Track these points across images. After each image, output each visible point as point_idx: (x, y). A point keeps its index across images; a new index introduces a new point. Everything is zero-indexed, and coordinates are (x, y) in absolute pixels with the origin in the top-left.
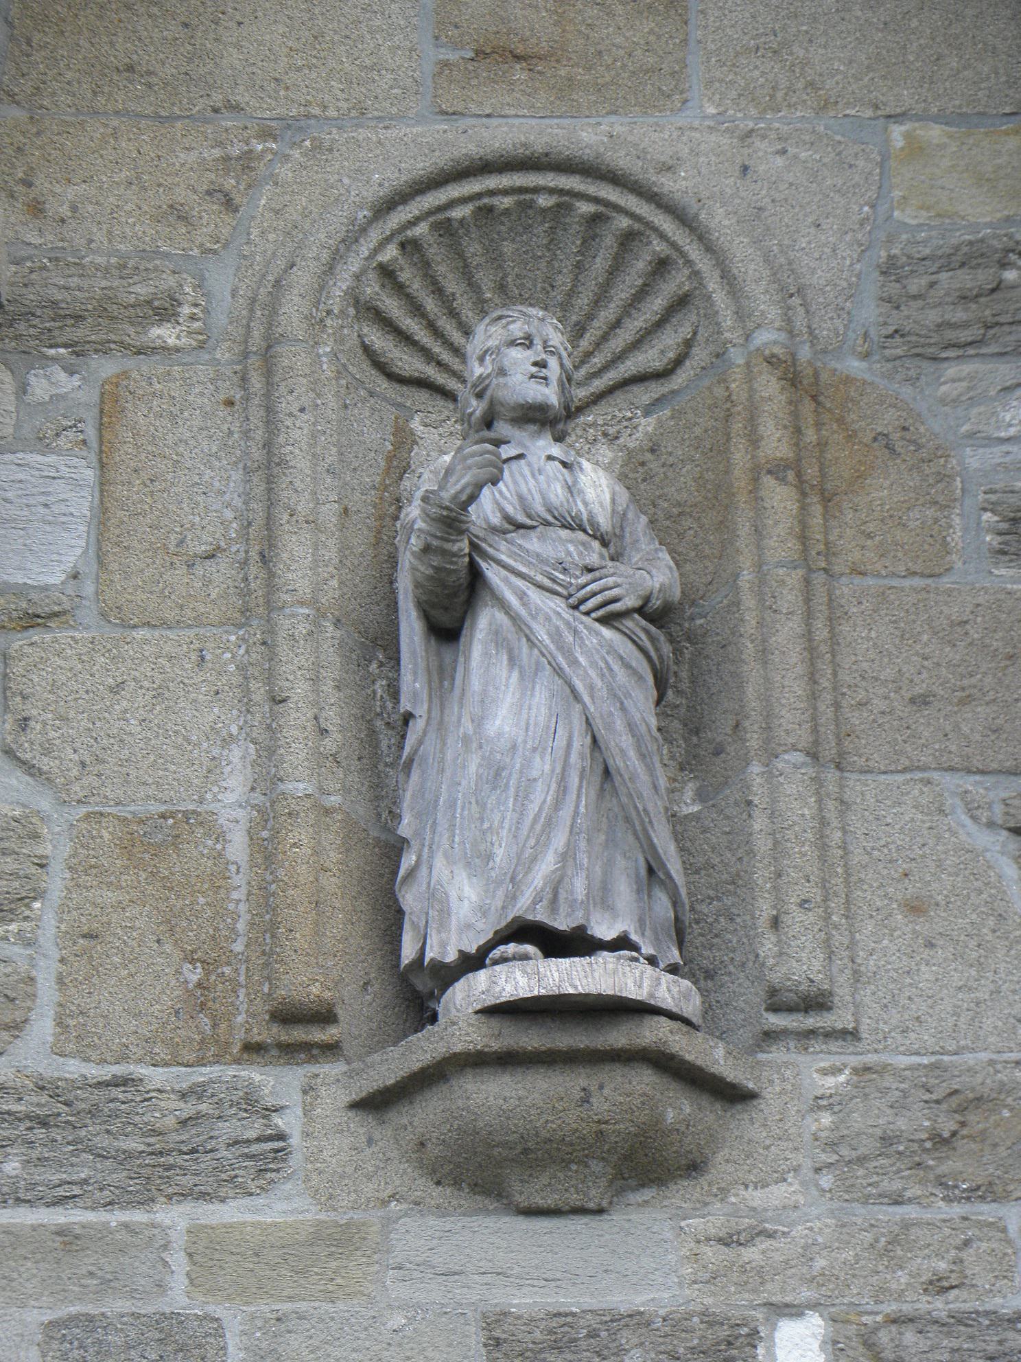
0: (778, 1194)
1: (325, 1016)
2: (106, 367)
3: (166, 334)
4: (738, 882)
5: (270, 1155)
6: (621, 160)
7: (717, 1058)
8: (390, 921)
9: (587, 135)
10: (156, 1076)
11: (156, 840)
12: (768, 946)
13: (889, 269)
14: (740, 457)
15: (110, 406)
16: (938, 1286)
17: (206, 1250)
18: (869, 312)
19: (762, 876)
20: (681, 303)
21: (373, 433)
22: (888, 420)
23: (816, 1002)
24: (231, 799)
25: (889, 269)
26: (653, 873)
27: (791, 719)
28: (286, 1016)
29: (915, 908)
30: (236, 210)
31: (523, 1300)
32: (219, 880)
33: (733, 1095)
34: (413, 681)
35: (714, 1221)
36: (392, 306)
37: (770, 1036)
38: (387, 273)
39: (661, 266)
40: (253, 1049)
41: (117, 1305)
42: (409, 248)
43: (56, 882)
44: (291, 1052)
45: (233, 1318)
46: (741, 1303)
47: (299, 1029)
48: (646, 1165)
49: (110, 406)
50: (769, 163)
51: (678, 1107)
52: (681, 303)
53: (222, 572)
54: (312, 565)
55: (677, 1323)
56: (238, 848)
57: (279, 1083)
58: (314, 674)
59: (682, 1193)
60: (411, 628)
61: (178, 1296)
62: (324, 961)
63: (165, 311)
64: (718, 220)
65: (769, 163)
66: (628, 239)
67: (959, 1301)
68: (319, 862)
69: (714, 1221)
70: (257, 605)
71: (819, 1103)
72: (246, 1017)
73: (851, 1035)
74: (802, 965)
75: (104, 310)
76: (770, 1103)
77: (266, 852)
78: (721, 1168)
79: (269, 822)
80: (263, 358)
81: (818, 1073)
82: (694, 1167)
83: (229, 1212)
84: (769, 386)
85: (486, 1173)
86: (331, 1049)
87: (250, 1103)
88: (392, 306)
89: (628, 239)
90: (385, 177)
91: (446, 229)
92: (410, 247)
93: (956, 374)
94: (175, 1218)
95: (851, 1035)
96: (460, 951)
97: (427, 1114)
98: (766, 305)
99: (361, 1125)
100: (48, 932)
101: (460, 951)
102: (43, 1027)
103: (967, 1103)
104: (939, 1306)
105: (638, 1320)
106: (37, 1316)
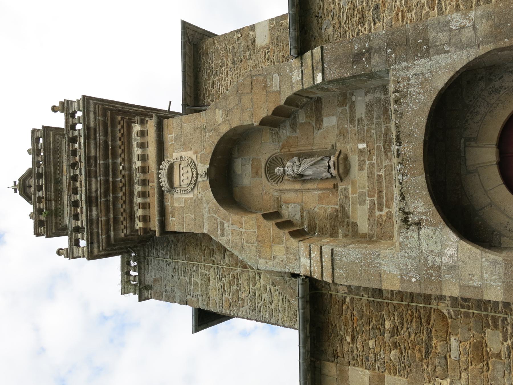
0: (348, 147)
1: (334, 184)
2: (282, 203)
3: (279, 198)
4: (323, 152)
5: (346, 188)
6: (265, 163)
7: (337, 153)
8: (327, 178)
9: (263, 166)
10: (339, 198)
11: (320, 198)
12: (328, 149)
13: (273, 142)
14: (288, 153)
15: (285, 203)
16: (355, 135)
17: (353, 193)
18: (277, 143)
19: (322, 150)
20: (276, 158)
21: (287, 182)
22: (285, 141)
23: (333, 145)
24: (317, 193)
25: (273, 142)
26: (322, 159)
27: (310, 148)
28: (334, 187)
29: (325, 138)
30: (400, 209)
31: (357, 168)
32: (323, 193)
33: (340, 152)
34: (307, 178)
35: (350, 153)
36: (277, 181)
37: (335, 149)
38: (274, 181)
39: (273, 160)
40: (337, 190)
41: (358, 200)
42: (481, 370)
43: (324, 206)
44: (337, 187)
45: (359, 191)
46: (357, 151)
47: (336, 187)
48: (346, 158)
49: (285, 203)
50: (265, 152)
51: (342, 156)
52: (276, 158)
53: (298, 193)
54: (298, 186)
55: (359, 156)
56: (321, 192)
57: (340, 188)
58: (309, 186)
59: (348, 156)
60: (303, 179)
61: (357, 195)
62: (330, 184)
63: (278, 198)
64: (269, 155)
65: (265, 152)
66: (271, 162)
67: (357, 133)
68: (322, 185)
69: (350, 153)
70: (301, 191)
71: (341, 145)
72: (334, 191)
73: (335, 143)
74: (330, 147)
75: (278, 203)
76: (341, 149)
77: (321, 189)
78: (346, 152)
79: (317, 189)
80: (281, 191)
81: (338, 145)
82: (346, 155)
83: (350, 192)
84: (282, 151)
85: (348, 170)
86: (337, 184)
87: (341, 190)
88: (277, 181)
89: (271, 162)
90: (267, 182)
91: (271, 177)
92: (272, 179)
93: (282, 136)
94: (351, 196)
95: (335, 143)
96: (123, 292)
97: (342, 176)
98: (276, 151)
99: (343, 181)
100: (328, 206)
101: (123, 292)
102: (336, 206)
103: (340, 133)
104: (357, 135)
105: (358, 159)
106: (359, 206)
